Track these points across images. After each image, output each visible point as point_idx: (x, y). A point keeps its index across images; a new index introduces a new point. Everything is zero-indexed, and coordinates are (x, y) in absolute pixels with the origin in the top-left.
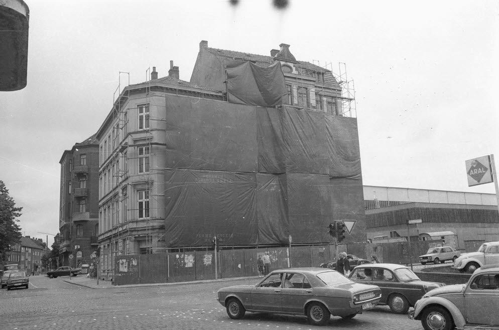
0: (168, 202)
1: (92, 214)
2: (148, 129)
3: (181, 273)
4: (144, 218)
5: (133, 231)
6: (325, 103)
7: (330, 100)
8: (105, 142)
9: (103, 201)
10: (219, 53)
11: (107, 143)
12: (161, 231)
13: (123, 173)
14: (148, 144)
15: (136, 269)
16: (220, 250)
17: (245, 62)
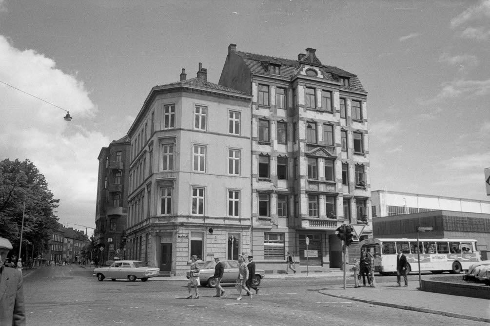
1: (125, 209)
9: (132, 196)
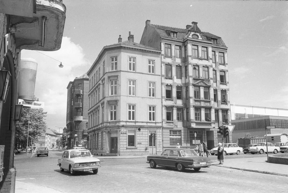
8: (97, 72)
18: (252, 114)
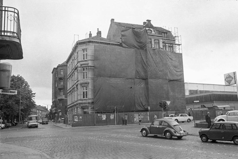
0: (95, 91)
2: (87, 59)
3: (100, 122)
4: (85, 98)
5: (80, 104)
6: (167, 47)
7: (170, 45)
8: (70, 65)
10: (119, 24)
11: (71, 65)
12: (92, 104)
13: (76, 79)
14: (87, 66)
15: (81, 120)
16: (117, 113)
17: (129, 29)
18: (203, 90)
